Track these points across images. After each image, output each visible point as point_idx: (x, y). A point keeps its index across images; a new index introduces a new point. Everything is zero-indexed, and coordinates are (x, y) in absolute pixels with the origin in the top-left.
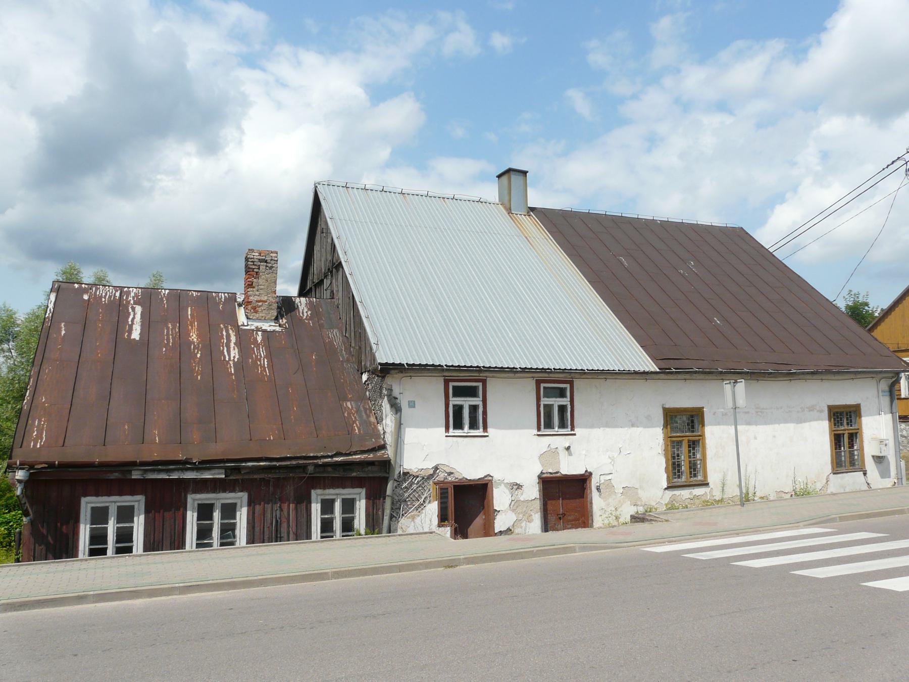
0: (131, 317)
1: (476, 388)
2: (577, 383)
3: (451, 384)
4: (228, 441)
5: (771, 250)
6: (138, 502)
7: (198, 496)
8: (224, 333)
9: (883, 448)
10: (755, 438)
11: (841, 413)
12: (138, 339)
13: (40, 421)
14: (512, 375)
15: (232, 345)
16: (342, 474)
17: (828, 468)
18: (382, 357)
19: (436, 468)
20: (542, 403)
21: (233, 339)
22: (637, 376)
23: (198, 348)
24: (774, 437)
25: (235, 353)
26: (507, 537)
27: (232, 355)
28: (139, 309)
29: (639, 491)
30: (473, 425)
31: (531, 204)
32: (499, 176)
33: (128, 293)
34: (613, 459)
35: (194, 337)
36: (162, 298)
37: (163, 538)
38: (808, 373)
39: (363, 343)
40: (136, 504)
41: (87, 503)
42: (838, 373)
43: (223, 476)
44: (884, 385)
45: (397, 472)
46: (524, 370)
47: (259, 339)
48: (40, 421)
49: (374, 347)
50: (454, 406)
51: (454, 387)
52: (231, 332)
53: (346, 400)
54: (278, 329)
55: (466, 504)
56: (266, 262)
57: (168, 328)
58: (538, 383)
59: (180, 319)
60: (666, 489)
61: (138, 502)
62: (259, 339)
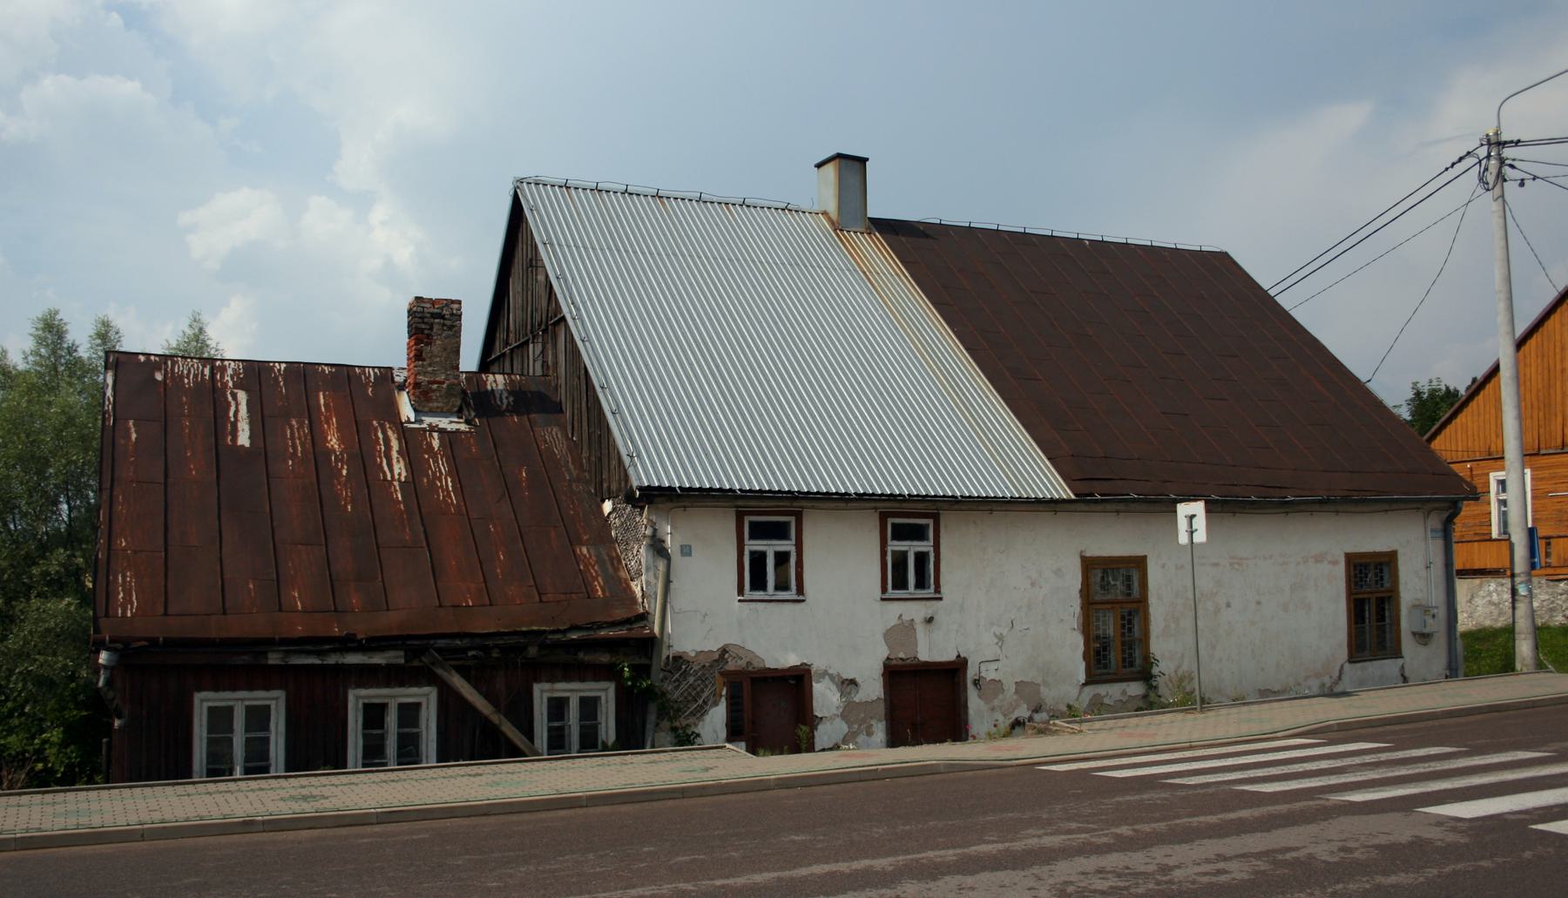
0: (233, 409)
1: (787, 524)
2: (945, 518)
3: (747, 520)
4: (407, 605)
5: (1272, 293)
6: (275, 701)
7: (363, 692)
8: (380, 435)
9: (1430, 621)
10: (1228, 605)
11: (1366, 566)
12: (247, 445)
13: (124, 577)
14: (842, 505)
15: (395, 454)
16: (567, 656)
17: (1343, 653)
18: (643, 475)
19: (724, 651)
20: (889, 549)
21: (395, 444)
22: (1024, 507)
23: (342, 460)
24: (1259, 603)
25: (400, 468)
26: (835, 753)
27: (396, 471)
28: (242, 396)
29: (1042, 688)
30: (782, 586)
31: (872, 213)
32: (819, 166)
33: (223, 369)
34: (1000, 638)
35: (333, 442)
36: (276, 378)
37: (316, 750)
38: (1313, 502)
39: (605, 451)
40: (273, 704)
41: (202, 701)
42: (1363, 501)
43: (402, 661)
44: (1435, 522)
45: (665, 653)
46: (861, 497)
47: (436, 444)
48: (124, 577)
49: (627, 460)
50: (752, 553)
51: (751, 523)
52: (390, 433)
53: (582, 544)
54: (463, 427)
55: (772, 705)
56: (443, 317)
57: (291, 427)
58: (883, 517)
59: (311, 412)
60: (1084, 685)
61: (275, 701)
62: (436, 444)
